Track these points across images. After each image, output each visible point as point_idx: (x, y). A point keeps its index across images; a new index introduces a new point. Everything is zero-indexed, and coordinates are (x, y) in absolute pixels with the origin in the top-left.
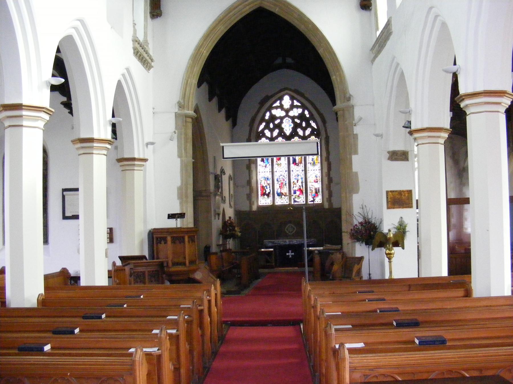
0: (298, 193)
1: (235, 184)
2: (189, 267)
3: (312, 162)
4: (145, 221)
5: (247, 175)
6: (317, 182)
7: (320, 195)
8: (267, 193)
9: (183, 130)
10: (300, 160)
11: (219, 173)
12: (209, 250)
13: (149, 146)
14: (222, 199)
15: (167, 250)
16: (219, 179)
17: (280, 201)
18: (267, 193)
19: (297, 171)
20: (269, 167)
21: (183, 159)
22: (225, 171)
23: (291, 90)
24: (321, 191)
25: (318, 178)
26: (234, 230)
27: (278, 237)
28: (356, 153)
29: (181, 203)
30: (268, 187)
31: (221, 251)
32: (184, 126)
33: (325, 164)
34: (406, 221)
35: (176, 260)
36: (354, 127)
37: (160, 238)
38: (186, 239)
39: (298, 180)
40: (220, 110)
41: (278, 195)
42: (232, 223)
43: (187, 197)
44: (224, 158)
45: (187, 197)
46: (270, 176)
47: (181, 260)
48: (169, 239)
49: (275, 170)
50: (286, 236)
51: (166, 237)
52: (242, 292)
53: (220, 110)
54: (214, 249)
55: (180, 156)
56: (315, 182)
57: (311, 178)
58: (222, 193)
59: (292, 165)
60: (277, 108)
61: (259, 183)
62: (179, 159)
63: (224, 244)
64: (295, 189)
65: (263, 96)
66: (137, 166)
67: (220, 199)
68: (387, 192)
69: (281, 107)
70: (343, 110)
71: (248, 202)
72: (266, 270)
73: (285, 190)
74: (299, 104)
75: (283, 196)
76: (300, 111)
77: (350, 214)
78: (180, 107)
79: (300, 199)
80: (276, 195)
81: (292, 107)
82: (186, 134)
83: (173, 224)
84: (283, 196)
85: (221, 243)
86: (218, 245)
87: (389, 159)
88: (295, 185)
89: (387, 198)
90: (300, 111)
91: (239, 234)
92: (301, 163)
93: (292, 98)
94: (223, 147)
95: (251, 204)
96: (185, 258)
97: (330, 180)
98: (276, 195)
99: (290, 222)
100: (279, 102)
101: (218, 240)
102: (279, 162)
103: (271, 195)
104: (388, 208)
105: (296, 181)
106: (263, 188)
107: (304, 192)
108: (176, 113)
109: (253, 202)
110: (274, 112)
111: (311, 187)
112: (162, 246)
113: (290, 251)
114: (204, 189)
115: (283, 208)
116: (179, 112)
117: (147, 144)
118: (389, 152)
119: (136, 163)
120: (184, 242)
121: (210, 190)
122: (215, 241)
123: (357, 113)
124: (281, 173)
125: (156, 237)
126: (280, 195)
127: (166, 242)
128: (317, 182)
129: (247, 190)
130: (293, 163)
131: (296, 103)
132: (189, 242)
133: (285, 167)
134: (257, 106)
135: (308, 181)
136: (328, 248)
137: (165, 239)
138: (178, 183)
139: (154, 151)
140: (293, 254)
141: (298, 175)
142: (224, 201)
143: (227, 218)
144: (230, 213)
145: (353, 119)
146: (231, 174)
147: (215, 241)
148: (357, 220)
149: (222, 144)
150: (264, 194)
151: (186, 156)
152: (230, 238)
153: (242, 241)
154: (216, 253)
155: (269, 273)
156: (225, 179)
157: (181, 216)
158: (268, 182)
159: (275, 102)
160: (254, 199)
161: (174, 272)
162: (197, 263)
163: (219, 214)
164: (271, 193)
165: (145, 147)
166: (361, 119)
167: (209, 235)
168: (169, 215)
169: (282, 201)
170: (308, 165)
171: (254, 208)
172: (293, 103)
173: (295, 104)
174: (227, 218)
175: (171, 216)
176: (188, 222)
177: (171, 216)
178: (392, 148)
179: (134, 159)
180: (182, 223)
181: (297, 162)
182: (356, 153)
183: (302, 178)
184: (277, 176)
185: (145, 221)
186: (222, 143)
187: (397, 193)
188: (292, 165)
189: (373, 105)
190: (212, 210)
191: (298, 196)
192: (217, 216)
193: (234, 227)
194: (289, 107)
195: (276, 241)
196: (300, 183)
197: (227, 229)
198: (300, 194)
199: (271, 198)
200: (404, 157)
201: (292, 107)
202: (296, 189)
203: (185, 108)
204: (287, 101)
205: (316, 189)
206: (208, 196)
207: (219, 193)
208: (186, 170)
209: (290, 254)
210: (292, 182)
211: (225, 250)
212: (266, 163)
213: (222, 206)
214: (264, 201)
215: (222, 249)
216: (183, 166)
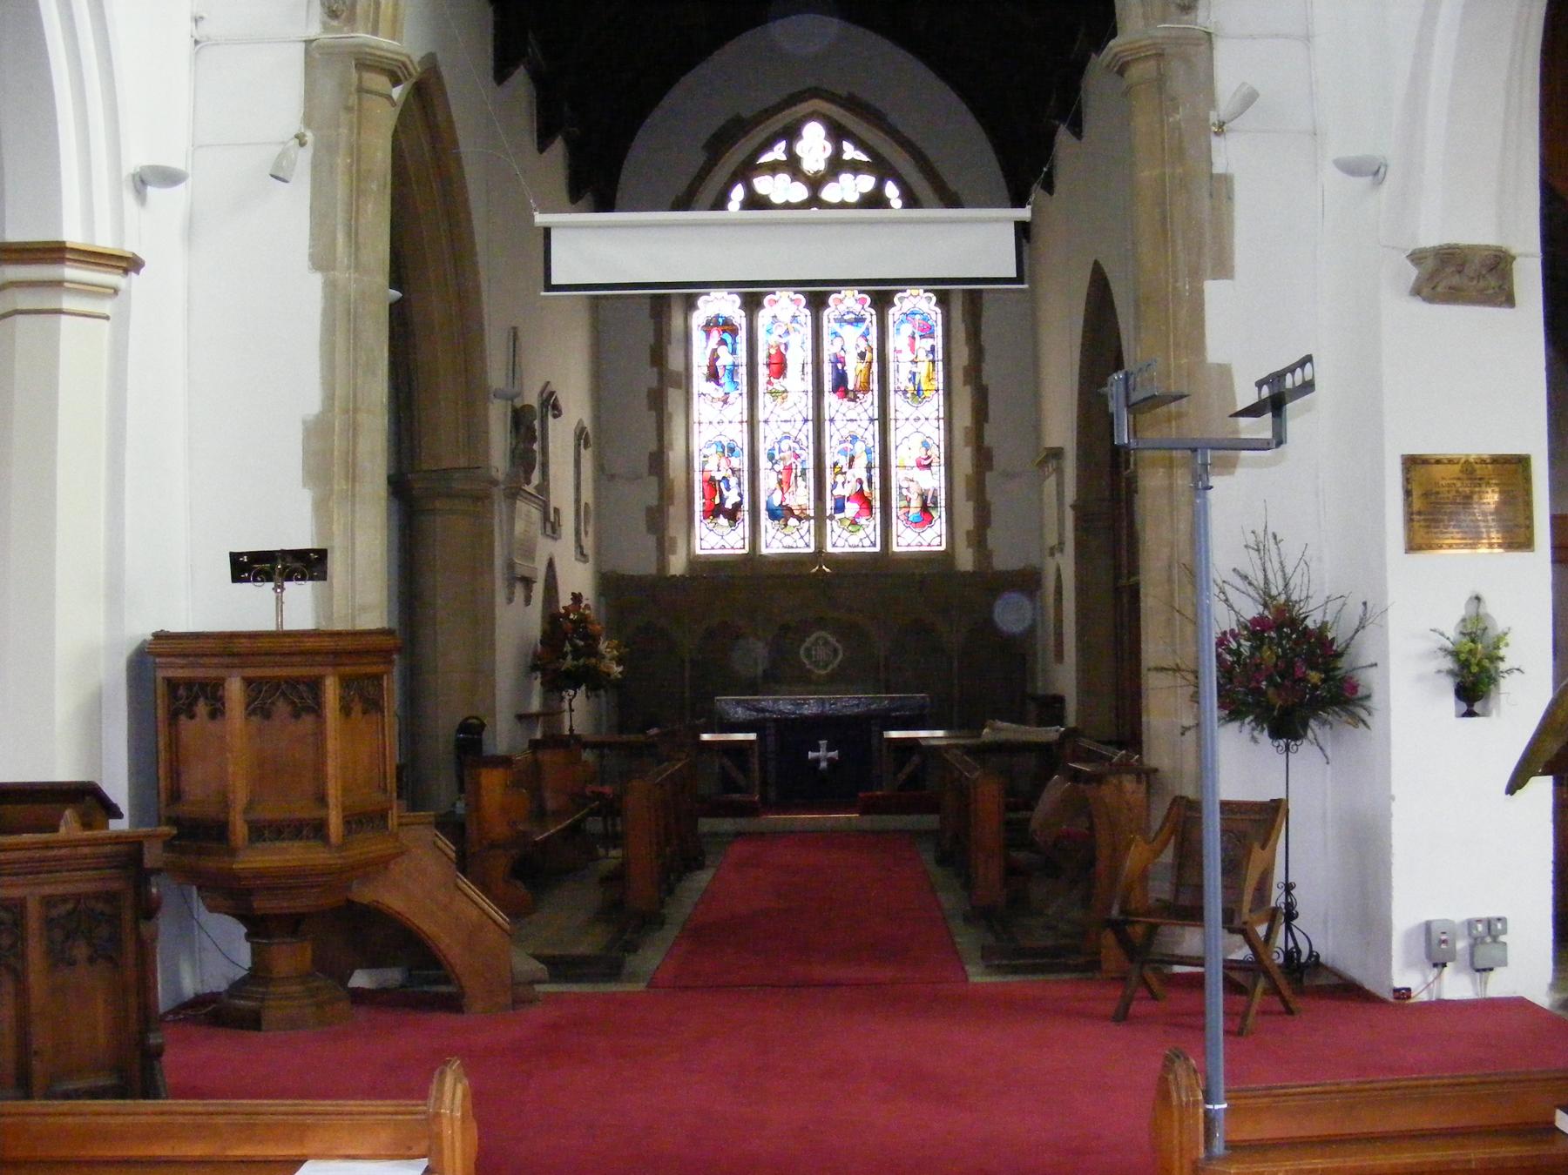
0: (852, 509)
1: (600, 468)
2: (342, 847)
3: (911, 387)
4: (115, 592)
5: (653, 434)
6: (929, 466)
7: (940, 515)
8: (728, 505)
9: (344, 131)
10: (862, 378)
11: (532, 399)
12: (480, 742)
13: (152, 192)
14: (546, 518)
15: (230, 750)
16: (531, 429)
17: (778, 541)
18: (728, 505)
19: (850, 420)
20: (739, 405)
21: (341, 275)
22: (562, 403)
23: (832, 98)
24: (942, 502)
25: (934, 452)
26: (591, 650)
27: (771, 680)
28: (1223, 269)
29: (322, 508)
30: (733, 481)
31: (535, 745)
32: (349, 109)
33: (964, 397)
34: (1500, 615)
35: (270, 811)
36: (1215, 141)
37: (189, 683)
38: (331, 690)
39: (852, 459)
40: (543, 144)
41: (774, 514)
42: (583, 620)
43: (352, 475)
44: (550, 287)
45: (352, 475)
46: (742, 440)
47: (302, 809)
48: (234, 689)
49: (762, 415)
50: (804, 681)
51: (219, 683)
52: (633, 962)
53: (543, 144)
54: (503, 737)
55: (321, 261)
56: (920, 466)
57: (905, 453)
58: (544, 488)
59: (831, 400)
60: (774, 168)
61: (697, 466)
62: (317, 279)
63: (550, 714)
64: (839, 491)
65: (718, 122)
66: (78, 292)
67: (536, 514)
68: (1412, 463)
69: (792, 166)
70: (1160, 56)
71: (651, 541)
72: (727, 825)
73: (801, 496)
74: (864, 158)
75: (793, 522)
76: (867, 183)
77: (1193, 571)
78: (333, 14)
79: (861, 534)
80: (764, 514)
81: (837, 166)
82: (357, 153)
83: (255, 609)
84: (793, 522)
85: (535, 705)
86: (522, 718)
87: (1417, 291)
88: (840, 478)
89: (1408, 493)
90: (867, 183)
91: (617, 670)
92: (866, 389)
93: (837, 133)
94: (547, 232)
95: (663, 548)
96: (322, 800)
97: (983, 458)
98: (764, 514)
99: (820, 623)
100: (782, 145)
101: (523, 693)
102: (778, 384)
103: (745, 515)
104: (1412, 547)
105: (843, 461)
106: (712, 484)
107: (877, 504)
108: (308, 42)
109: (673, 541)
110: (763, 184)
111: (905, 484)
112: (194, 729)
113: (823, 743)
114: (462, 462)
115: (790, 565)
116: (326, 38)
117: (140, 182)
118: (1417, 257)
119: (71, 272)
120: (317, 709)
121: (488, 468)
122: (507, 701)
123: (1231, 70)
124: (786, 427)
125: (176, 682)
126: (781, 514)
127: (217, 712)
128: (929, 466)
129: (648, 494)
130: (835, 390)
131: (850, 152)
132: (346, 710)
133: (801, 406)
134: (700, 158)
135: (893, 462)
136: (1002, 736)
137: (212, 691)
138: (310, 400)
139: (191, 229)
140: (834, 754)
141: (854, 438)
142: (551, 526)
143: (565, 600)
144: (577, 579)
145: (1212, 102)
146: (587, 424)
147: (507, 701)
148: (1230, 611)
149: (541, 219)
150: (714, 511)
151: (357, 265)
152: (576, 687)
153: (629, 704)
154: (505, 762)
155: (739, 834)
156: (560, 436)
157: (306, 564)
158: (735, 463)
159: (768, 145)
160: (675, 529)
161: (259, 874)
162: (393, 821)
163: (528, 582)
164: (746, 506)
165: (129, 198)
166: (1250, 99)
167: (481, 673)
168: (235, 558)
169: (788, 541)
170: (895, 400)
171: (677, 565)
172: (838, 151)
173: (846, 157)
174: (565, 600)
175: (247, 567)
176: (358, 595)
177: (247, 567)
178: (1432, 237)
179: (55, 252)
180: (324, 604)
181: (851, 386)
182: (1223, 269)
183: (868, 452)
184: (768, 437)
185: (115, 592)
186: (544, 211)
187: (1457, 468)
188: (831, 400)
189: (1308, 38)
190: (499, 562)
191: (854, 523)
192: (519, 591)
193: (596, 639)
194: (821, 166)
195: (766, 701)
196: (859, 471)
197: (563, 651)
198: (858, 515)
199: (743, 528)
200: (1492, 282)
201: (837, 166)
202: (847, 491)
203: (360, 22)
204: (814, 145)
205: (923, 496)
206: (481, 498)
207: (530, 489)
208: (355, 335)
209: (822, 754)
210: (829, 462)
211: (556, 741)
212: (728, 387)
213: (545, 548)
214: (716, 540)
215: (538, 735)
216: (339, 316)
